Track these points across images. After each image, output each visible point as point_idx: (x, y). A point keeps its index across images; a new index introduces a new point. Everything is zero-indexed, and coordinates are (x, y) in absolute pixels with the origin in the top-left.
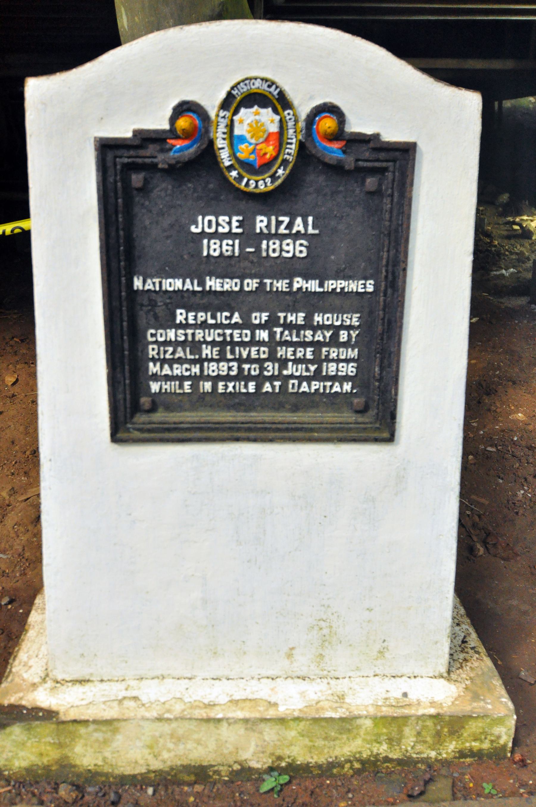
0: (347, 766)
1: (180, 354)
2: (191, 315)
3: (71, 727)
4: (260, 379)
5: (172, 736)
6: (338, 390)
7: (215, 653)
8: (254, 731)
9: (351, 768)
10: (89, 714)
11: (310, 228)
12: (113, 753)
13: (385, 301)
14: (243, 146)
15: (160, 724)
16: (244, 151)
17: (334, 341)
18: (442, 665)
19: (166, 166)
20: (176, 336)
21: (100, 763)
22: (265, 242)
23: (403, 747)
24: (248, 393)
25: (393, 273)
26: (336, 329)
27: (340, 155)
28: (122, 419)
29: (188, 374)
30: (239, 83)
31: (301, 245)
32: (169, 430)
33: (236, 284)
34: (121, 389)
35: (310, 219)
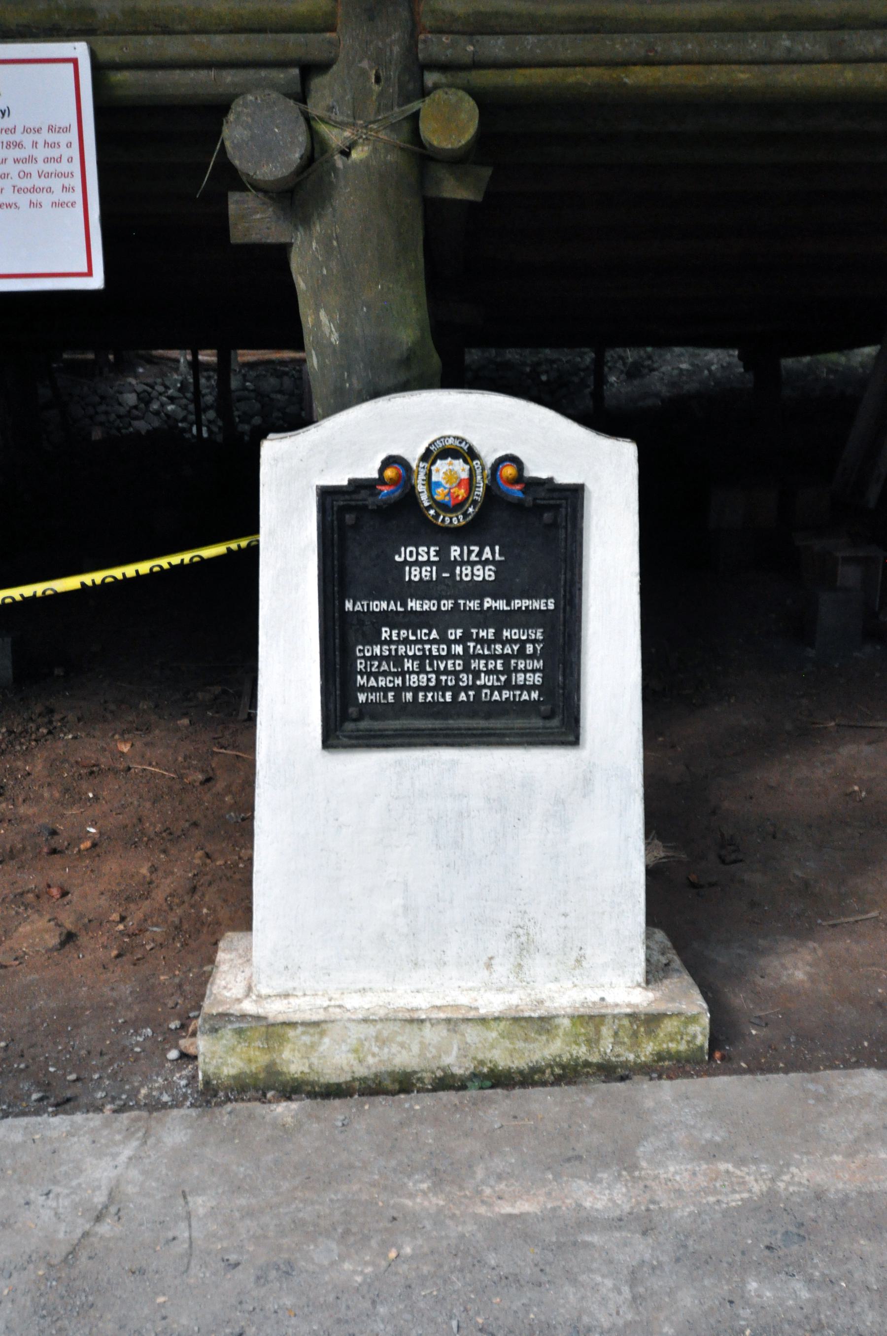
0: (548, 1071)
1: (384, 667)
2: (395, 632)
3: (280, 1030)
4: (456, 690)
5: (377, 1038)
6: (527, 698)
7: (416, 964)
8: (455, 1032)
9: (552, 1073)
10: (297, 1017)
11: (497, 555)
12: (320, 1058)
13: (564, 617)
14: (440, 490)
15: (366, 1026)
16: (440, 494)
17: (522, 654)
18: (640, 978)
19: (375, 507)
20: (381, 650)
21: (306, 1070)
22: (458, 568)
23: (602, 1049)
24: (445, 702)
25: (571, 592)
26: (523, 644)
27: (521, 495)
28: (333, 727)
29: (391, 685)
30: (435, 441)
31: (490, 570)
32: (374, 737)
33: (434, 605)
34: (332, 698)
35: (497, 548)
